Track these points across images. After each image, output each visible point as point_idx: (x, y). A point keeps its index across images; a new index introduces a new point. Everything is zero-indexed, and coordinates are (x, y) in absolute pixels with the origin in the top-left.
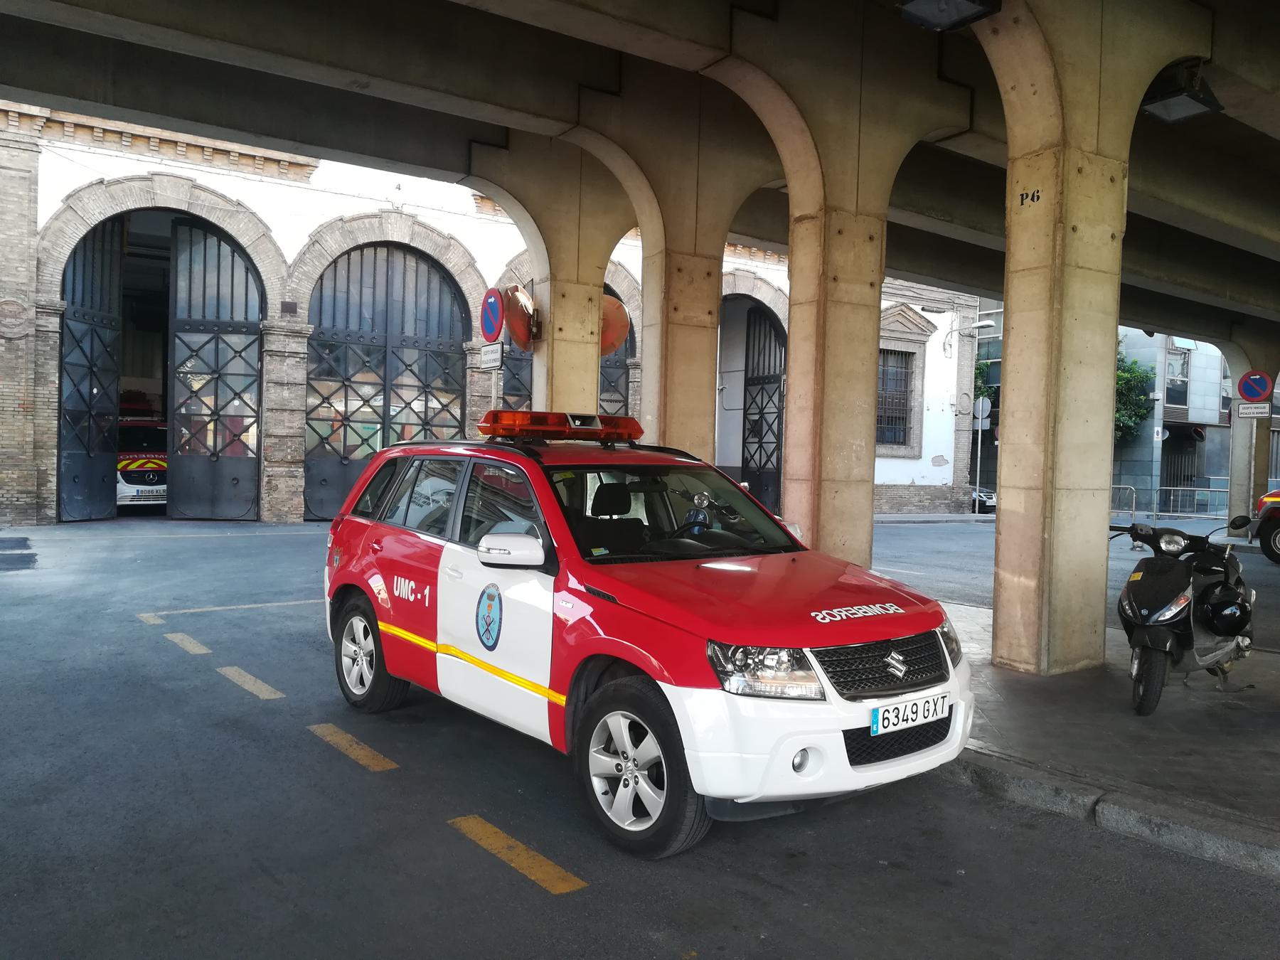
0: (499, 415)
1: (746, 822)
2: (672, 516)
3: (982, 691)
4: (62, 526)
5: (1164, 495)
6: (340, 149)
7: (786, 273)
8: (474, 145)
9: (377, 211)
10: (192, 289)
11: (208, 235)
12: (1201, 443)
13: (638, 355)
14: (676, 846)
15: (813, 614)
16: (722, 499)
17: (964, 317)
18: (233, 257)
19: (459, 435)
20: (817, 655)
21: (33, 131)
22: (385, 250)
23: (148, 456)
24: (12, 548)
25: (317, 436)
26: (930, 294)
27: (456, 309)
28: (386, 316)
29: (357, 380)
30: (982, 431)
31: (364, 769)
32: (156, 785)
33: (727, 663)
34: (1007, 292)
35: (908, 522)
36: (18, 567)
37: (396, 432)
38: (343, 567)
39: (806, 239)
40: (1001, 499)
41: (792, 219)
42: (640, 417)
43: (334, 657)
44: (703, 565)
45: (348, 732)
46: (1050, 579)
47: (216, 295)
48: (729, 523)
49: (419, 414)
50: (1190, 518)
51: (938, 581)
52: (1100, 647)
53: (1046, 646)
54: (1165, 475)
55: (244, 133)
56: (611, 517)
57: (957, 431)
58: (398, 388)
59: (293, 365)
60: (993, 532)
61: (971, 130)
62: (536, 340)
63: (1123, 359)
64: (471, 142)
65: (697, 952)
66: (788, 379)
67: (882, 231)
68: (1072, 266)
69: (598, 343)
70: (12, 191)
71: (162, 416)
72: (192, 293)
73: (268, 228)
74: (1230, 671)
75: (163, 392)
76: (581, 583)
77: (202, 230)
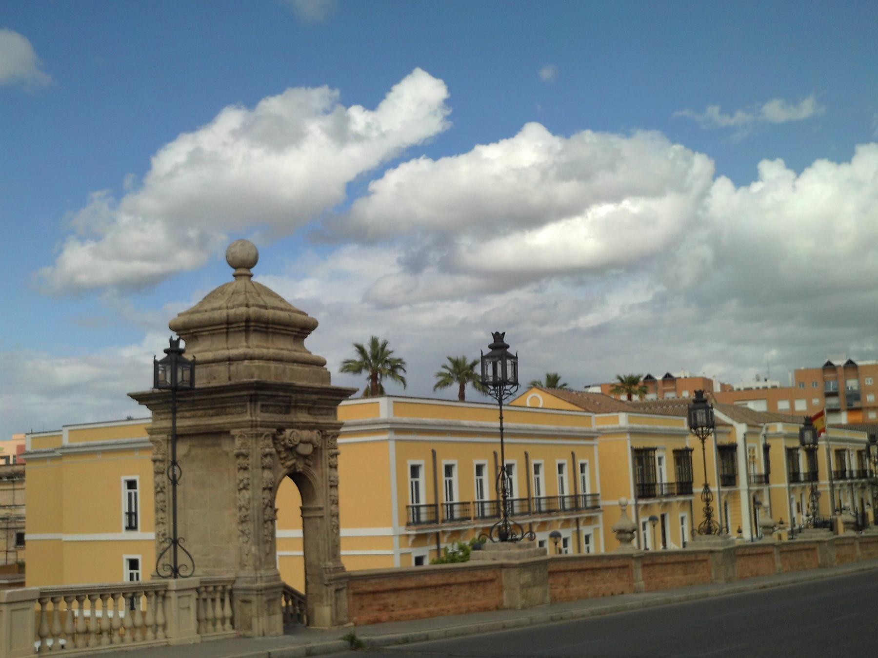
0: (807, 478)
3: (540, 144)
13: (127, 493)
16: (519, 608)
17: (355, 594)
19: (505, 531)
24: (709, 419)
25: (704, 480)
35: (447, 494)
36: (182, 429)
39: (385, 359)
41: (665, 551)
43: (871, 453)
45: (674, 141)
49: (489, 535)
52: (852, 455)
53: (11, 509)
56: (792, 406)
58: (377, 345)
59: (223, 290)
63: (270, 533)
70: (62, 642)
71: (858, 472)
74: (838, 385)
76: (793, 99)
77: (449, 90)
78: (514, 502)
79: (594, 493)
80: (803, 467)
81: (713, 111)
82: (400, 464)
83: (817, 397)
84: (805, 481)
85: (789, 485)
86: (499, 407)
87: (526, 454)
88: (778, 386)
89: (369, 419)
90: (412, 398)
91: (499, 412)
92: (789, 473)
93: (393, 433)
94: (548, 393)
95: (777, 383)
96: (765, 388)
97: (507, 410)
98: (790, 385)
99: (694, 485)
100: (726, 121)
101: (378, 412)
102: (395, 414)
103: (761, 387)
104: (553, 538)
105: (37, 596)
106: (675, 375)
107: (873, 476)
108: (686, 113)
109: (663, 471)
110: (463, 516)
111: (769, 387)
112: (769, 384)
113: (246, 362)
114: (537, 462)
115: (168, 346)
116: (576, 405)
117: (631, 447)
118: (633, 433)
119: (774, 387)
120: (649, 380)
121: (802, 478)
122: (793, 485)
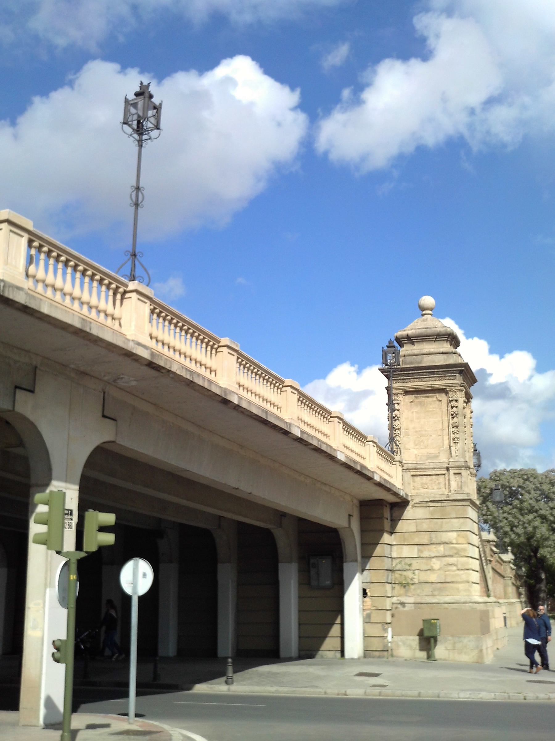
1: (355, 539)
2: (430, 371)
6: (138, 632)
7: (218, 393)
8: (18, 392)
9: (61, 667)
12: (475, 462)
20: (38, 720)
21: (456, 563)
23: (438, 627)
26: (426, 383)
29: (220, 351)
30: (126, 695)
34: (344, 542)
37: (133, 118)
40: (452, 352)
42: (150, 316)
47: (484, 604)
54: (425, 379)
55: (169, 694)
57: (125, 102)
61: (120, 319)
62: (515, 483)
64: (16, 387)
67: (216, 691)
69: (380, 695)
78: (484, 538)
115: (388, 344)
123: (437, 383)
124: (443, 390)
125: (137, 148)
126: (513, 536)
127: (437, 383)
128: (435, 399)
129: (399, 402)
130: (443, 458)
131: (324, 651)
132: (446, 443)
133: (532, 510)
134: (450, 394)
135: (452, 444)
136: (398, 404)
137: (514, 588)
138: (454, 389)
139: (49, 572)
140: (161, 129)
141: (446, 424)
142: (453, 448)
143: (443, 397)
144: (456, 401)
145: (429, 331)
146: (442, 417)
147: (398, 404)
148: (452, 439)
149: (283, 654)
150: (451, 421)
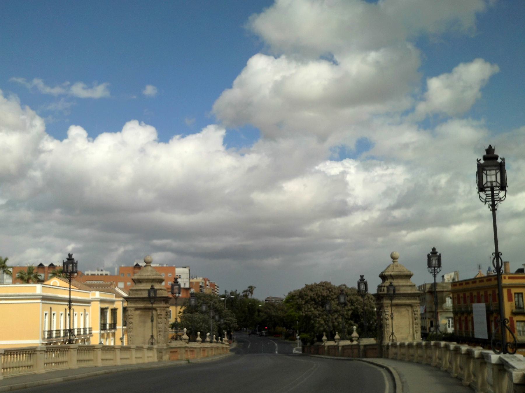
4: (42, 332)
5: (456, 302)
10: (86, 322)
11: (69, 299)
14: (52, 107)
15: (224, 331)
18: (523, 305)
22: (477, 336)
27: (511, 335)
28: (520, 330)
31: (251, 344)
32: (165, 324)
33: (58, 344)
35: (45, 326)
38: (517, 330)
44: (472, 362)
46: (127, 350)
48: (285, 301)
50: (315, 357)
51: (410, 333)
60: (68, 290)
65: (209, 332)
66: (461, 385)
68: (55, 330)
72: (87, 307)
73: (429, 257)
75: (496, 251)
76: (90, 85)
79: (79, 328)
80: (109, 321)
81: (38, 82)
82: (43, 312)
83: (129, 282)
84: (110, 329)
85: (100, 331)
86: (69, 289)
87: (51, 308)
88: (109, 274)
89: (31, 293)
90: (65, 287)
91: (69, 291)
92: (101, 324)
93: (27, 386)
94: (62, 280)
95: (108, 273)
96: (101, 275)
97: (73, 291)
98: (116, 274)
99: (117, 325)
100: (48, 90)
101: (35, 291)
102: (100, 296)
103: (99, 275)
104: (121, 340)
105: (3, 352)
106: (55, 264)
107: (453, 299)
108: (20, 80)
109: (61, 321)
110: (314, 345)
111: (104, 274)
112: (104, 273)
113: (160, 291)
114: (54, 313)
116: (76, 287)
117: (100, 307)
118: (102, 301)
119: (106, 275)
120: (41, 266)
121: (108, 327)
122: (102, 332)
123: (408, 302)
124: (411, 305)
125: (434, 278)
126: (326, 327)
127: (408, 302)
128: (405, 309)
129: (388, 310)
130: (410, 340)
131: (151, 331)
132: (411, 332)
133: (337, 311)
134: (414, 307)
135: (415, 333)
136: (388, 311)
137: (499, 194)
138: (416, 305)
139: (138, 299)
140: (424, 283)
141: (411, 323)
142: (415, 335)
143: (410, 309)
144: (417, 311)
145: (402, 274)
146: (409, 318)
147: (388, 311)
148: (415, 330)
149: (4, 283)
150: (414, 321)
